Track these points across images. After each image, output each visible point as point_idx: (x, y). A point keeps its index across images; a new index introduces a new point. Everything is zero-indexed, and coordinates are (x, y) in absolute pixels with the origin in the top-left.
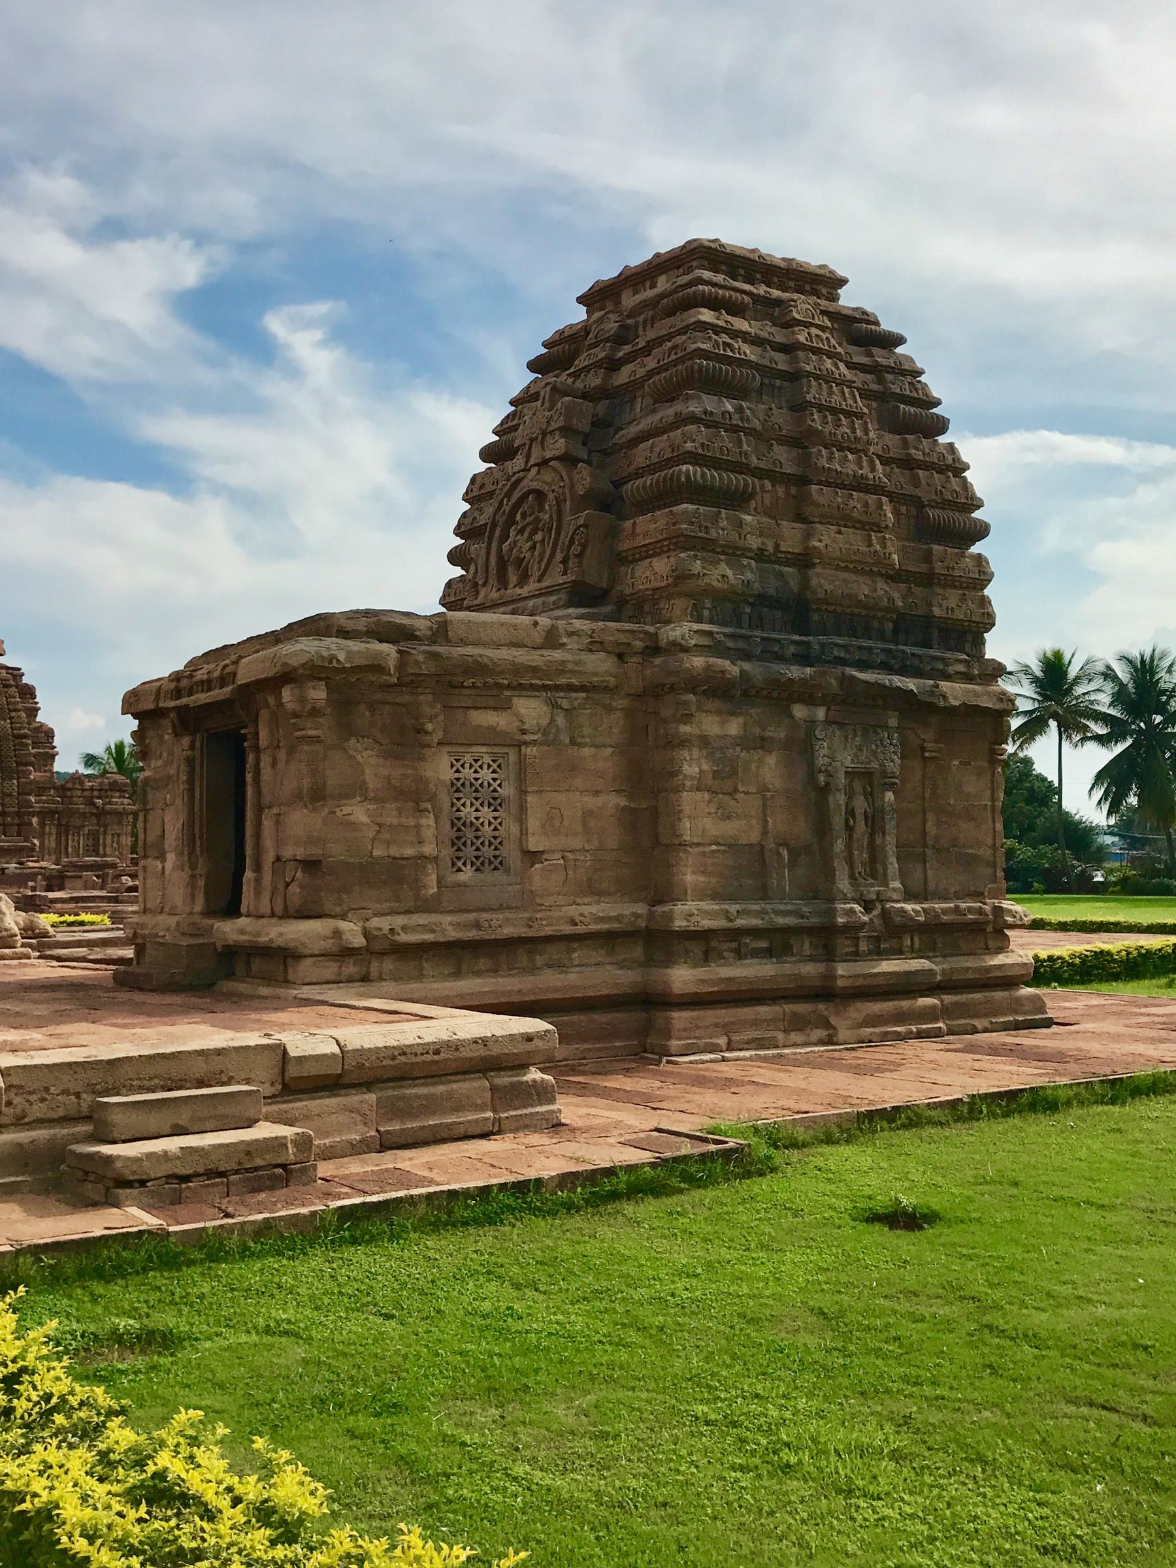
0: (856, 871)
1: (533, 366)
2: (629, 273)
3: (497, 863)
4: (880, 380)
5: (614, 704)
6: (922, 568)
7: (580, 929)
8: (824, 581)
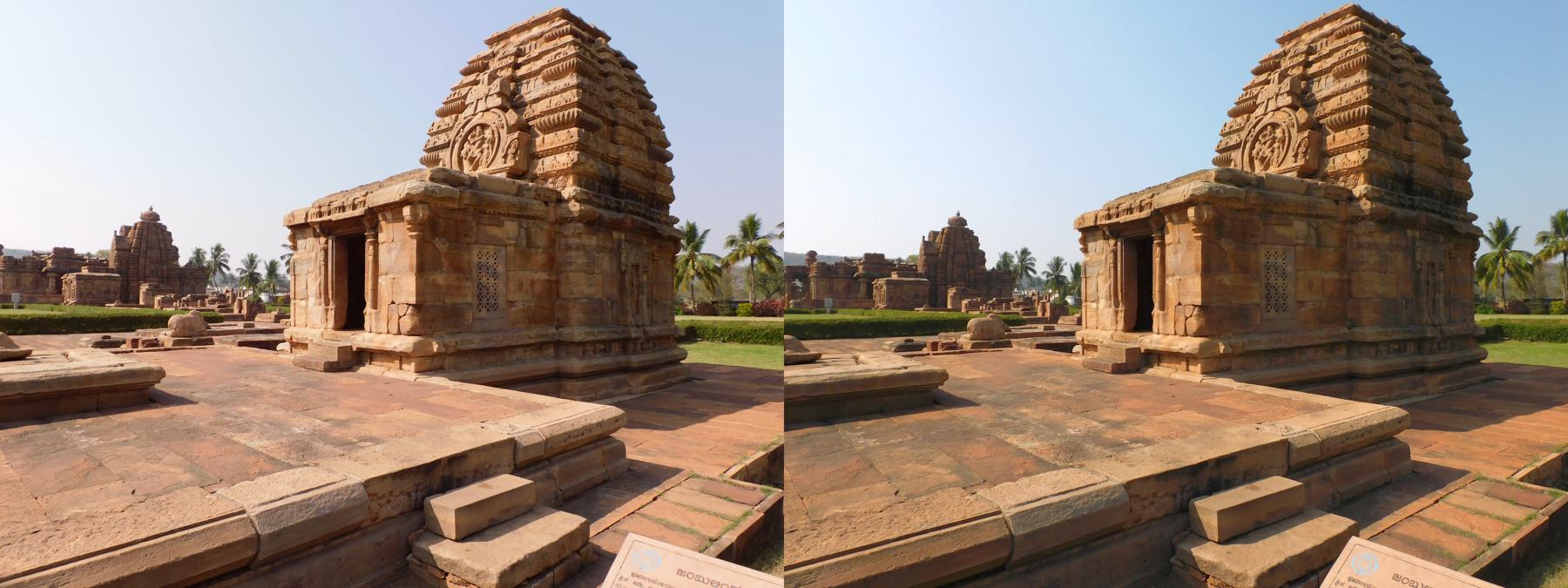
3: (1284, 308)
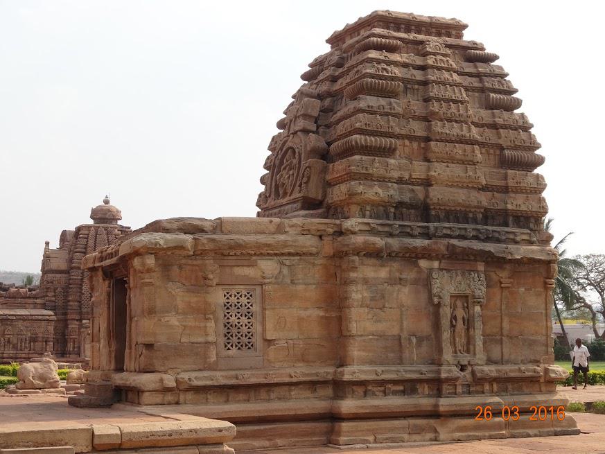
0: (457, 349)
1: (304, 77)
2: (348, 28)
3: (250, 346)
4: (481, 81)
5: (316, 262)
6: (503, 183)
7: (294, 380)
8: (436, 194)
